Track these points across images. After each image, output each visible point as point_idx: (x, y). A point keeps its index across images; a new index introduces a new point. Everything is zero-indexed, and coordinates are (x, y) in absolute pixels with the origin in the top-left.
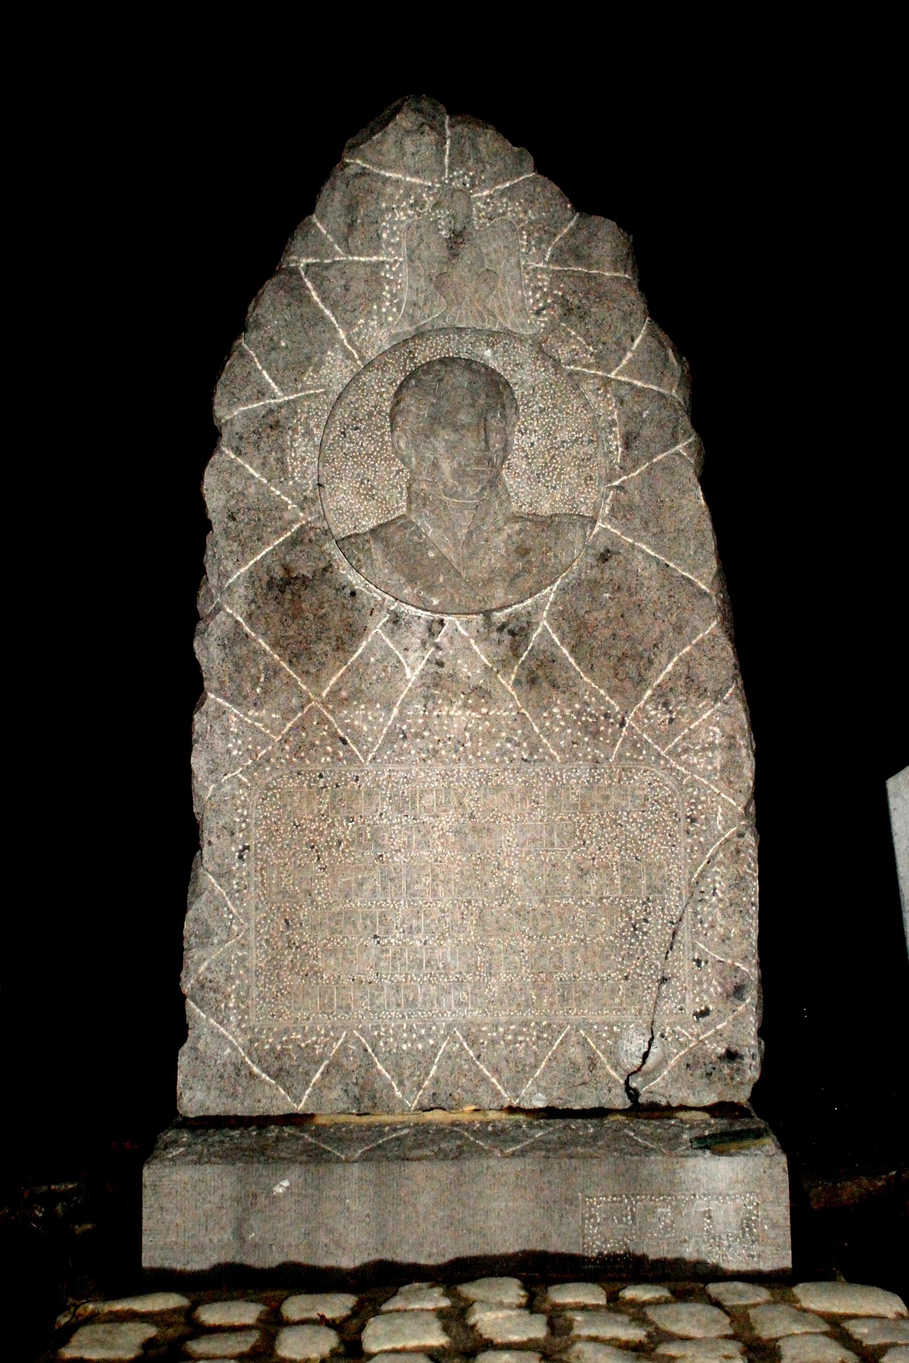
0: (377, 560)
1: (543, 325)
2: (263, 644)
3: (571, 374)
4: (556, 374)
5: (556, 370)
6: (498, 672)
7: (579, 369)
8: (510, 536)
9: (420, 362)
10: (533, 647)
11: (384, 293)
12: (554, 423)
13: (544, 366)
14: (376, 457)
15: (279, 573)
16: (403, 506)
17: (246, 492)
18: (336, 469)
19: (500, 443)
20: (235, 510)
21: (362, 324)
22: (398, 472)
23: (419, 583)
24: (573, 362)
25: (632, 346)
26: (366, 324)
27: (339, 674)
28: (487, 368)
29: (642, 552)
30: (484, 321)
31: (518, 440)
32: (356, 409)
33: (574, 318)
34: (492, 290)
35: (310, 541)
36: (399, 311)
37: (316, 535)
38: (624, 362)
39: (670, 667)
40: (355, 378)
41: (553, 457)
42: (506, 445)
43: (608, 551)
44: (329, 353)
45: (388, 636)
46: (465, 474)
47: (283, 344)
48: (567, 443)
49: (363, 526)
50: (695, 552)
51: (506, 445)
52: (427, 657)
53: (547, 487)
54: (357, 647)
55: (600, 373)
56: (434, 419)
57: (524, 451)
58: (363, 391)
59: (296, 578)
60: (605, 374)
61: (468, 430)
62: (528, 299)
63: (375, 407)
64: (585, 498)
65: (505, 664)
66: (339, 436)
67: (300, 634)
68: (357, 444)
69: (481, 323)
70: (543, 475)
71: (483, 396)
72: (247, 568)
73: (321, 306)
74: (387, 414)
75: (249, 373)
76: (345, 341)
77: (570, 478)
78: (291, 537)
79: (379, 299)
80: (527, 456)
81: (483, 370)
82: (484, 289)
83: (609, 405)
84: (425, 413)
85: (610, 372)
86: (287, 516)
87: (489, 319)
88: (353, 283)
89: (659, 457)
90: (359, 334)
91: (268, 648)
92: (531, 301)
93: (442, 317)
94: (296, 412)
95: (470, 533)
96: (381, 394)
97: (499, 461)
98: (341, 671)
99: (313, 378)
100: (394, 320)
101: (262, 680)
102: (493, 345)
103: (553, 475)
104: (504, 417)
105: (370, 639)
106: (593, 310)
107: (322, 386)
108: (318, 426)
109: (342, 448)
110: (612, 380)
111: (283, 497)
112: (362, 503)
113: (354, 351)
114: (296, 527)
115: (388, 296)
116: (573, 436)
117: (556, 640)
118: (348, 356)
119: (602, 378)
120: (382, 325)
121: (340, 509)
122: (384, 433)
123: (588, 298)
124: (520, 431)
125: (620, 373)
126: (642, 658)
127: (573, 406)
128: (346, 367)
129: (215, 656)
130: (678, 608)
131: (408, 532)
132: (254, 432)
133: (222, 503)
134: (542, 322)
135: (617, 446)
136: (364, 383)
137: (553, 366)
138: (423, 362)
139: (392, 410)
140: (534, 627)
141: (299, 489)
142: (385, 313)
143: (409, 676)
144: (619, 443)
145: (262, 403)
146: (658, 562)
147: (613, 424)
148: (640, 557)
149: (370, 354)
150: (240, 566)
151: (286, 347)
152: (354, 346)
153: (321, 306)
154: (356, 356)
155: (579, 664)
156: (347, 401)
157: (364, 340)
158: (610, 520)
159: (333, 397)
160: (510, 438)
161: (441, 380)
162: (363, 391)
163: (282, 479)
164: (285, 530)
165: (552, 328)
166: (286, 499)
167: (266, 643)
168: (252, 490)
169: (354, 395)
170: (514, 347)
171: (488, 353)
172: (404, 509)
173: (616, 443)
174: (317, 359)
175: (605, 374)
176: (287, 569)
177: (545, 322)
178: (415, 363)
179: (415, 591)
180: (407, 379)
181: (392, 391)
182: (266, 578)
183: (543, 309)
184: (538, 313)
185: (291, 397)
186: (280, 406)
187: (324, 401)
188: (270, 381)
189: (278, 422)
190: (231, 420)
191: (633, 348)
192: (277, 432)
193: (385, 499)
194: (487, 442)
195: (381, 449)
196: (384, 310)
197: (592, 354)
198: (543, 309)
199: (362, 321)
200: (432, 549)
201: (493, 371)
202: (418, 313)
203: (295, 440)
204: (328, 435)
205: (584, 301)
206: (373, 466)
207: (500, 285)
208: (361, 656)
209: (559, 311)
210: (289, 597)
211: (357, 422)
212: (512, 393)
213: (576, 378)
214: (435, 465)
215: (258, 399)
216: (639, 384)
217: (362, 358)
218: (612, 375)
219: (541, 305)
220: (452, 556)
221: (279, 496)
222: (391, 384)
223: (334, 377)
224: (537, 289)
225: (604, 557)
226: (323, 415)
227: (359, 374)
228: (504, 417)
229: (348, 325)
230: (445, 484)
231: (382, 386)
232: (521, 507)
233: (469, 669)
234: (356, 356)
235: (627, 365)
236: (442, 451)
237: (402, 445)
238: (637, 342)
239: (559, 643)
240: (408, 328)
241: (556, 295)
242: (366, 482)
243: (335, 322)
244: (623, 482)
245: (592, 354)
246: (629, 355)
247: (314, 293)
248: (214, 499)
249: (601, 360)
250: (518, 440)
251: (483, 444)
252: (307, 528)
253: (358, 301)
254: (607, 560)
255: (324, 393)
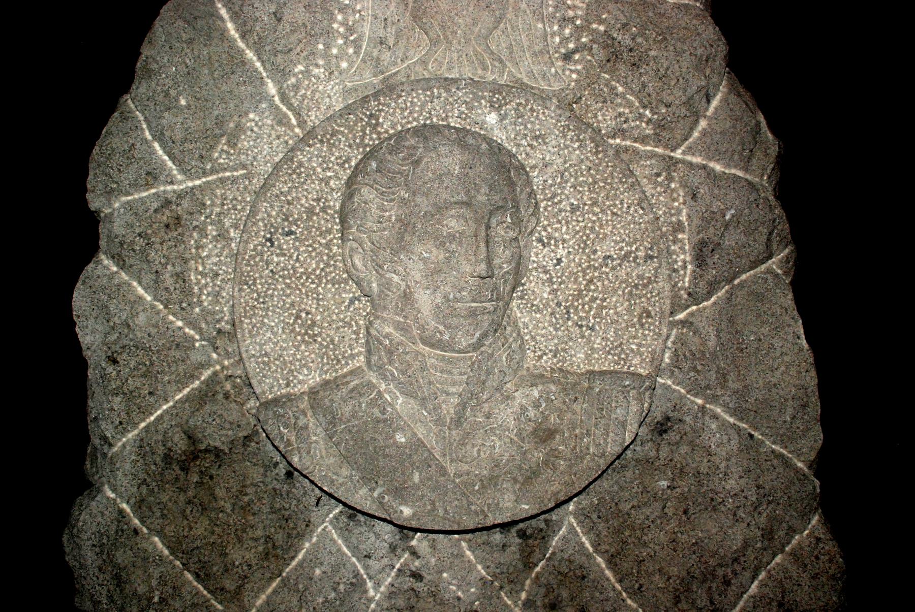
0: (316, 442)
1: (574, 76)
2: (160, 545)
3: (618, 150)
4: (597, 153)
5: (597, 146)
6: (501, 588)
7: (628, 143)
8: (523, 409)
9: (386, 132)
10: (554, 553)
11: (335, 26)
12: (592, 228)
13: (579, 140)
14: (319, 277)
15: (180, 443)
16: (361, 352)
17: (130, 321)
18: (259, 295)
19: (510, 262)
20: (117, 348)
21: (302, 72)
22: (352, 302)
23: (380, 482)
24: (619, 132)
25: (707, 109)
26: (307, 73)
27: (270, 590)
28: (490, 141)
29: (715, 417)
30: (485, 68)
31: (537, 255)
32: (289, 203)
33: (622, 67)
34: (499, 20)
35: (227, 396)
36: (356, 53)
37: (234, 386)
38: (696, 134)
39: (754, 588)
40: (288, 158)
41: (591, 281)
42: (519, 264)
43: (668, 419)
44: (251, 116)
45: (341, 535)
46: (454, 313)
47: (183, 102)
48: (613, 260)
49: (300, 382)
50: (794, 417)
51: (519, 264)
52: (398, 566)
53: (581, 326)
54: (297, 553)
55: (660, 150)
56: (405, 226)
57: (546, 272)
58: (299, 175)
59: (207, 451)
60: (667, 152)
61: (460, 243)
62: (552, 37)
63: (318, 200)
64: (640, 345)
65: (513, 582)
66: (263, 245)
67: (213, 533)
68: (291, 257)
69: (480, 72)
70: (576, 309)
71: (484, 189)
72: (136, 432)
73: (241, 44)
74: (336, 212)
75: (133, 145)
76: (277, 99)
77: (617, 313)
78: (199, 390)
79: (329, 33)
80: (550, 281)
81: (484, 146)
82: (487, 19)
83: (674, 200)
84: (392, 214)
85: (673, 150)
86: (196, 357)
87: (494, 66)
88: (286, 11)
89: (744, 277)
90: (296, 87)
91: (166, 552)
92: (557, 39)
93: (423, 62)
94: (204, 204)
95: (463, 406)
96: (326, 180)
97: (508, 288)
98: (274, 585)
99: (228, 153)
100: (351, 66)
101: (156, 599)
102: (500, 106)
103: (591, 308)
104: (518, 222)
105: (314, 539)
106: (652, 53)
107: (244, 167)
108: (236, 227)
109: (268, 263)
110: (678, 161)
111: (187, 330)
112: (297, 348)
113: (290, 114)
114: (206, 374)
115: (342, 30)
116: (621, 249)
117: (588, 545)
118: (282, 120)
119: (663, 157)
120: (331, 73)
121: (266, 355)
122: (331, 240)
123: (643, 35)
124: (540, 240)
125: (690, 150)
126: (714, 577)
127: (622, 203)
128: (278, 137)
129: (89, 562)
130: (769, 502)
131: (364, 400)
132: (140, 235)
133: (99, 337)
134: (572, 74)
135: (685, 262)
136: (301, 164)
137: (593, 140)
138: (392, 132)
139: (343, 205)
140: (556, 529)
141: (209, 319)
142: (337, 57)
143: (371, 593)
144: (688, 259)
145: (153, 191)
146: (739, 430)
147: (678, 227)
148: (713, 426)
149: (313, 118)
150: (125, 431)
151: (188, 107)
152: (290, 107)
153: (241, 44)
154: (294, 121)
155: (620, 581)
156: (276, 191)
157: (304, 96)
158: (672, 372)
159: (257, 183)
160: (524, 254)
161: (417, 163)
162: (299, 175)
163: (184, 305)
164: (193, 377)
165: (589, 80)
166: (192, 332)
167: (163, 543)
168: (141, 319)
169: (285, 182)
170: (532, 110)
171: (492, 118)
172: (362, 358)
173: (684, 257)
174: (232, 125)
175: (667, 152)
176: (191, 438)
177: (578, 72)
178: (379, 133)
179: (376, 494)
180: (367, 157)
181: (345, 175)
182: (161, 450)
183: (574, 52)
184: (567, 57)
185: (198, 182)
186: (180, 196)
187: (245, 188)
188: (166, 158)
189: (178, 218)
190: (112, 214)
191: (709, 113)
192: (175, 234)
193: (332, 341)
194: (489, 261)
195: (328, 265)
196: (335, 51)
197: (649, 121)
198: (574, 52)
199: (300, 68)
200: (403, 430)
201: (500, 147)
202: (386, 56)
203: (202, 247)
204: (246, 242)
205: (639, 40)
206: (315, 291)
207: (510, 15)
208: (300, 565)
209: (600, 54)
210: (196, 478)
211: (290, 223)
212: (529, 182)
213: (624, 156)
214: (407, 297)
215: (148, 186)
216: (718, 168)
217: (302, 124)
218: (678, 154)
219: (571, 46)
220: (432, 442)
221: (180, 328)
222: (342, 165)
223: (260, 152)
224: (565, 21)
225: (662, 428)
226: (243, 209)
227: (292, 150)
228: (518, 222)
229: (280, 74)
230: (422, 328)
231: (329, 169)
232: (540, 357)
233: (459, 587)
234: (294, 121)
235: (700, 139)
236: (418, 277)
237: (358, 263)
238: (715, 103)
239: (591, 549)
240: (371, 79)
241: (596, 31)
242: (304, 315)
243: (261, 69)
244: (692, 314)
245: (649, 121)
246: (703, 124)
247: (230, 25)
248: (87, 331)
249: (662, 131)
250: (537, 254)
251: (483, 266)
252: (222, 376)
253: (293, 38)
254: (666, 431)
255: (245, 176)
